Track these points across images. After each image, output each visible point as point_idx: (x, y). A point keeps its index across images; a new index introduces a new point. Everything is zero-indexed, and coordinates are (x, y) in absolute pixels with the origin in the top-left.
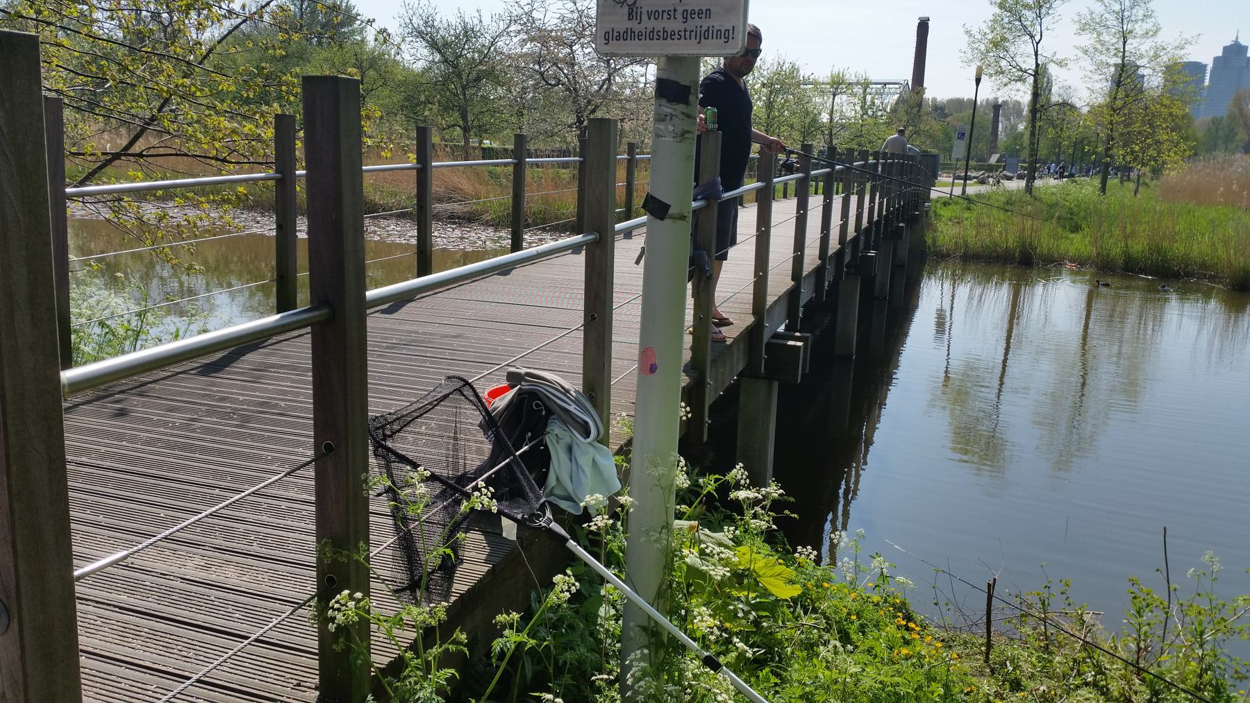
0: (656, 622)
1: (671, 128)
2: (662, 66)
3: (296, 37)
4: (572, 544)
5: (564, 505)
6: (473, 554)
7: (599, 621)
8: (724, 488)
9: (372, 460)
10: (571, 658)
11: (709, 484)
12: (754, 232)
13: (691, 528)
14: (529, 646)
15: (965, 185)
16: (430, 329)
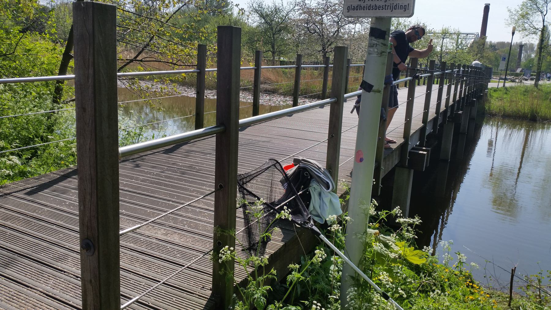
0: (359, 274)
1: (376, 50)
2: (374, 22)
3: (205, 12)
4: (322, 236)
5: (316, 219)
6: (276, 237)
7: (330, 272)
8: (389, 217)
9: (238, 195)
10: (317, 287)
11: (383, 214)
12: (406, 100)
13: (375, 234)
14: (301, 279)
15: (504, 83)
16: (258, 139)
